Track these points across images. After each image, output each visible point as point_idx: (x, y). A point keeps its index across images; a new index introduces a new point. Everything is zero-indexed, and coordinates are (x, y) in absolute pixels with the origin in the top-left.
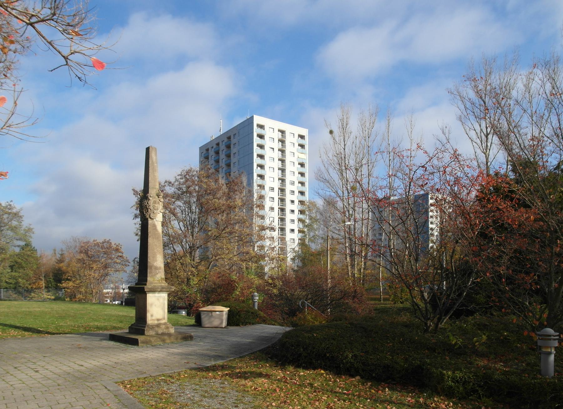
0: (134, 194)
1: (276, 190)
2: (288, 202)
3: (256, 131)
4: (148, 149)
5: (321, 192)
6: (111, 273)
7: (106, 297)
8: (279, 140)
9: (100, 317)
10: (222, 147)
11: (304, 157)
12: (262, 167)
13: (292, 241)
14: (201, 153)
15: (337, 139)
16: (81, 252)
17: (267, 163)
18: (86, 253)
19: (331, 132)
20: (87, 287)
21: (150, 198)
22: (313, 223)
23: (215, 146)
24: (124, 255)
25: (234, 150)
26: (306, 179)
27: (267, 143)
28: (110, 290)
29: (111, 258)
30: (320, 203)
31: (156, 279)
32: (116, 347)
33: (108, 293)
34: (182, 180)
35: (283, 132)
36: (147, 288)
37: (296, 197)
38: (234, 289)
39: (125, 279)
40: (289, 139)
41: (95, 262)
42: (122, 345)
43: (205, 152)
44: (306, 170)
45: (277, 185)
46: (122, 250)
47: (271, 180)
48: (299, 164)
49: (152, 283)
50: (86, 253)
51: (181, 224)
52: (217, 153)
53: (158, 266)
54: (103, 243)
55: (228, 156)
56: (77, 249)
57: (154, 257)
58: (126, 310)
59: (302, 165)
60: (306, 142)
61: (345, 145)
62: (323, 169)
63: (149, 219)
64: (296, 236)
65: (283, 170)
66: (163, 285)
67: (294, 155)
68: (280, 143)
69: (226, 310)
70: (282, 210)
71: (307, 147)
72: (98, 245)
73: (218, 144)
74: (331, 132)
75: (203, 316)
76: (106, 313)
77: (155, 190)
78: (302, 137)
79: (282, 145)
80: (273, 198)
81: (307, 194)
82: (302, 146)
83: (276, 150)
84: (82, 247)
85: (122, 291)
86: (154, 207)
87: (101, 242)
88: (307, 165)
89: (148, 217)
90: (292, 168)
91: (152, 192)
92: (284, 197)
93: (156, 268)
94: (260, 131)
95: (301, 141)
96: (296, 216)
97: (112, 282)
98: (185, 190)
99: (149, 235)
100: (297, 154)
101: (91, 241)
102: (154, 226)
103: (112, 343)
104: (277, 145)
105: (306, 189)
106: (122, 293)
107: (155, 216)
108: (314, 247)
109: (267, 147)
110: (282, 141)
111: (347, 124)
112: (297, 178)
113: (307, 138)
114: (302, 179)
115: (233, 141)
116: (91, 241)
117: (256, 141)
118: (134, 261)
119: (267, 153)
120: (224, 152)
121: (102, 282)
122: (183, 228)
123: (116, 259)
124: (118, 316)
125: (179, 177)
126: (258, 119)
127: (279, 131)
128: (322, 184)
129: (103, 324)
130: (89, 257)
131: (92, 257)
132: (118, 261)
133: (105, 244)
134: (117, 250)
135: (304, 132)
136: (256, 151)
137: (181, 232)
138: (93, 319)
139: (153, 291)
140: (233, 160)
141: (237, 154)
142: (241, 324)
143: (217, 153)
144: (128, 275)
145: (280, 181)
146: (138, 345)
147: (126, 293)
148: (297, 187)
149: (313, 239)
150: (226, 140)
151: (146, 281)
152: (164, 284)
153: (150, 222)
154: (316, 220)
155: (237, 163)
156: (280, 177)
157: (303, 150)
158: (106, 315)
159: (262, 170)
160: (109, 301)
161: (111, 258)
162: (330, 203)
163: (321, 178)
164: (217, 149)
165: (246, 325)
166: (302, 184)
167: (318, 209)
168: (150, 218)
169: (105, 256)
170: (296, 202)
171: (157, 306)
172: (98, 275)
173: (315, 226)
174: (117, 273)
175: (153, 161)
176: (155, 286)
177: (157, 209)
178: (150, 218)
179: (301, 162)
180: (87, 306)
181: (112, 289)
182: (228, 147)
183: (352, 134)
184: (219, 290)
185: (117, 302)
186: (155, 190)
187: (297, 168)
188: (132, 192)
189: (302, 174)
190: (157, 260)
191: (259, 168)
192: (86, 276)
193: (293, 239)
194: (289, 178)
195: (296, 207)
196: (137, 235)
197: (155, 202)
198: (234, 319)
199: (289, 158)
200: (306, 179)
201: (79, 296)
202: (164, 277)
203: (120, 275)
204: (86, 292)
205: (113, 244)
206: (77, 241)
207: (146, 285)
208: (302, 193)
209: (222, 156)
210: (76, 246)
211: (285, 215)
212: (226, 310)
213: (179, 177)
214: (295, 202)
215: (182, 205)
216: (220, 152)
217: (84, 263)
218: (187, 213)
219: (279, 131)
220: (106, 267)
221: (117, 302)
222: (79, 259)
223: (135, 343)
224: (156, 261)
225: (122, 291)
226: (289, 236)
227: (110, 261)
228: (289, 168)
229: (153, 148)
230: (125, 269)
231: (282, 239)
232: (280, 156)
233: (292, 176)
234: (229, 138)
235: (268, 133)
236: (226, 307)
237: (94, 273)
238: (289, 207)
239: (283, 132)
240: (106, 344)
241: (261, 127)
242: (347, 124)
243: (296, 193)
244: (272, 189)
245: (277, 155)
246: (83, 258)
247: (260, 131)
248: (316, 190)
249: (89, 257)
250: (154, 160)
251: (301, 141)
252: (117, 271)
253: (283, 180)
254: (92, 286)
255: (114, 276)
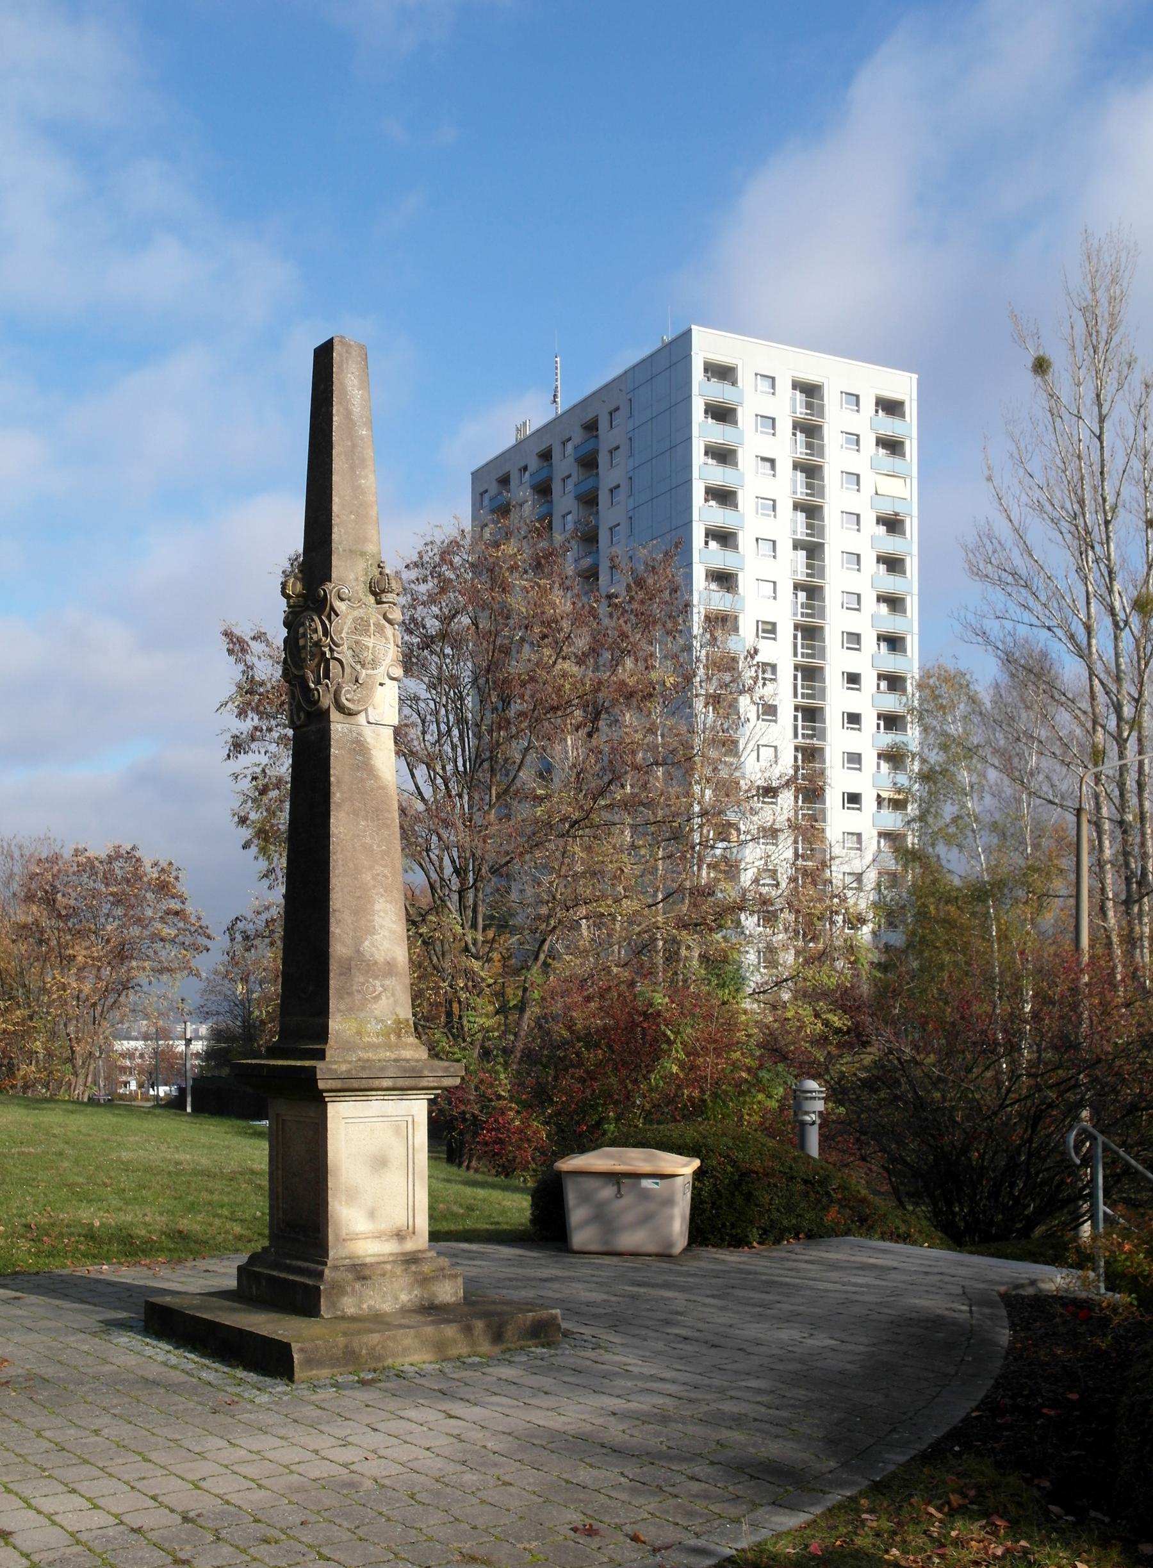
0: (230, 652)
1: (786, 631)
2: (833, 680)
3: (702, 391)
4: (324, 357)
5: (994, 627)
6: (142, 978)
7: (123, 1070)
8: (798, 426)
9: (102, 1177)
10: (564, 464)
11: (901, 490)
12: (724, 537)
13: (851, 842)
14: (479, 496)
15: (1065, 393)
16: (30, 898)
17: (749, 521)
18: (49, 901)
19: (1041, 366)
20: (54, 1034)
21: (340, 606)
22: (954, 760)
23: (534, 464)
24: (189, 908)
25: (609, 475)
26: (909, 585)
27: (750, 440)
28: (140, 1044)
29: (139, 921)
30: (985, 673)
31: (373, 1027)
32: (177, 1376)
33: (129, 1055)
34: (423, 588)
35: (810, 391)
36: (327, 1071)
37: (868, 661)
38: (656, 1048)
39: (194, 1000)
40: (836, 420)
41: (79, 934)
42: (212, 1372)
43: (493, 488)
44: (909, 546)
45: (785, 611)
46: (182, 888)
47: (764, 596)
48: (881, 520)
49: (349, 1047)
50: (49, 901)
51: (421, 771)
52: (543, 490)
53: (380, 957)
54: (111, 859)
55: (589, 500)
56: (15, 886)
57: (362, 910)
58: (204, 1140)
59: (892, 524)
60: (908, 428)
61: (1102, 419)
62: (1004, 531)
63: (334, 715)
64: (868, 821)
65: (813, 550)
66: (407, 1054)
67: (862, 484)
68: (800, 436)
69: (685, 1167)
70: (811, 715)
71: (911, 448)
72: (89, 867)
73: (546, 455)
74: (1041, 366)
75: (571, 1197)
76: (125, 1155)
77: (361, 565)
78: (891, 407)
79: (809, 446)
80: (858, 636)
81: (912, 644)
82: (892, 446)
83: (785, 466)
84: (32, 877)
85: (180, 1047)
86: (357, 650)
87: (103, 855)
88: (912, 526)
89: (326, 701)
90: (850, 539)
91: (347, 576)
92: (816, 662)
93: (370, 968)
94: (719, 392)
95: (890, 426)
96: (869, 739)
97: (147, 1016)
98: (433, 626)
99: (336, 796)
100: (869, 480)
101: (67, 854)
102: (360, 749)
103: (158, 1356)
104: (786, 447)
105: (909, 624)
106: (184, 1056)
107: (365, 700)
108: (961, 866)
109: (746, 458)
110: (810, 430)
111: (1112, 327)
112: (870, 579)
113: (911, 410)
114: (891, 584)
115: (608, 437)
116: (67, 854)
117: (703, 431)
118: (231, 929)
119: (749, 481)
120: (570, 483)
121: (110, 1015)
122: (428, 792)
123: (159, 926)
124: (177, 1171)
125: (413, 574)
126: (707, 345)
127: (797, 385)
128: (997, 596)
129: (112, 1220)
130: (59, 916)
131: (68, 917)
132: (168, 931)
133: (116, 865)
134: (163, 888)
135: (902, 385)
136: (704, 473)
137: (420, 807)
138: (71, 1186)
139: (358, 1087)
140: (609, 514)
141: (623, 490)
142: (754, 1234)
143: (543, 490)
144: (203, 985)
145: (802, 596)
146: (291, 1379)
147: (197, 1055)
148: (870, 619)
149: (952, 830)
150: (578, 436)
151: (322, 1034)
152: (414, 1051)
153: (338, 726)
154: (971, 752)
155: (622, 530)
156: (801, 577)
157: (897, 460)
158: (126, 1167)
159: (729, 554)
160: (133, 1086)
161: (139, 921)
162: (1030, 673)
163: (996, 566)
164: (543, 475)
165: (778, 1241)
166: (894, 603)
167: (973, 700)
168: (341, 709)
169: (119, 911)
170: (869, 680)
171: (380, 1169)
172: (95, 990)
173: (965, 777)
174: (165, 977)
175: (348, 414)
176: (366, 1064)
177: (374, 664)
178: (341, 709)
179: (888, 510)
180: (52, 1118)
181: (146, 1037)
182: (589, 463)
183: (1137, 367)
184: (593, 1057)
185: (162, 1091)
186: (361, 565)
187: (871, 539)
188: (223, 644)
189: (893, 564)
190: (374, 926)
191: (713, 544)
192: (48, 992)
193: (857, 838)
194: (837, 580)
195: (868, 701)
196: (243, 821)
197: (361, 626)
198: (719, 1217)
199: (836, 499)
200: (909, 585)
201: (27, 1070)
202: (405, 1012)
203: (179, 987)
204: (50, 1055)
205: (147, 864)
206: (17, 855)
207: (321, 1055)
208: (894, 642)
209: (565, 501)
210: (11, 876)
211: (821, 734)
212: (685, 1167)
213: (413, 574)
214: (864, 680)
215: (424, 695)
216: (556, 487)
217: (40, 942)
218: (443, 727)
219: (797, 385)
220: (122, 954)
221: (162, 1091)
222: (24, 926)
223: (273, 1361)
224: (371, 931)
225: (180, 1047)
226: (838, 822)
227: (135, 931)
228: (837, 538)
229: (342, 343)
230: (193, 964)
231: (809, 830)
232: (801, 493)
233: (850, 580)
234: (591, 427)
235: (750, 400)
236: (679, 1150)
237: (80, 979)
238: (837, 700)
239: (810, 391)
240: (132, 1360)
241: (722, 373)
242: (1112, 327)
243: (869, 641)
244: (769, 629)
245: (787, 486)
246: (36, 922)
247: (719, 392)
248: (971, 618)
249: (59, 916)
250: (356, 409)
251: (890, 426)
252: (161, 971)
253: (812, 592)
254: (71, 1029)
255: (155, 991)
